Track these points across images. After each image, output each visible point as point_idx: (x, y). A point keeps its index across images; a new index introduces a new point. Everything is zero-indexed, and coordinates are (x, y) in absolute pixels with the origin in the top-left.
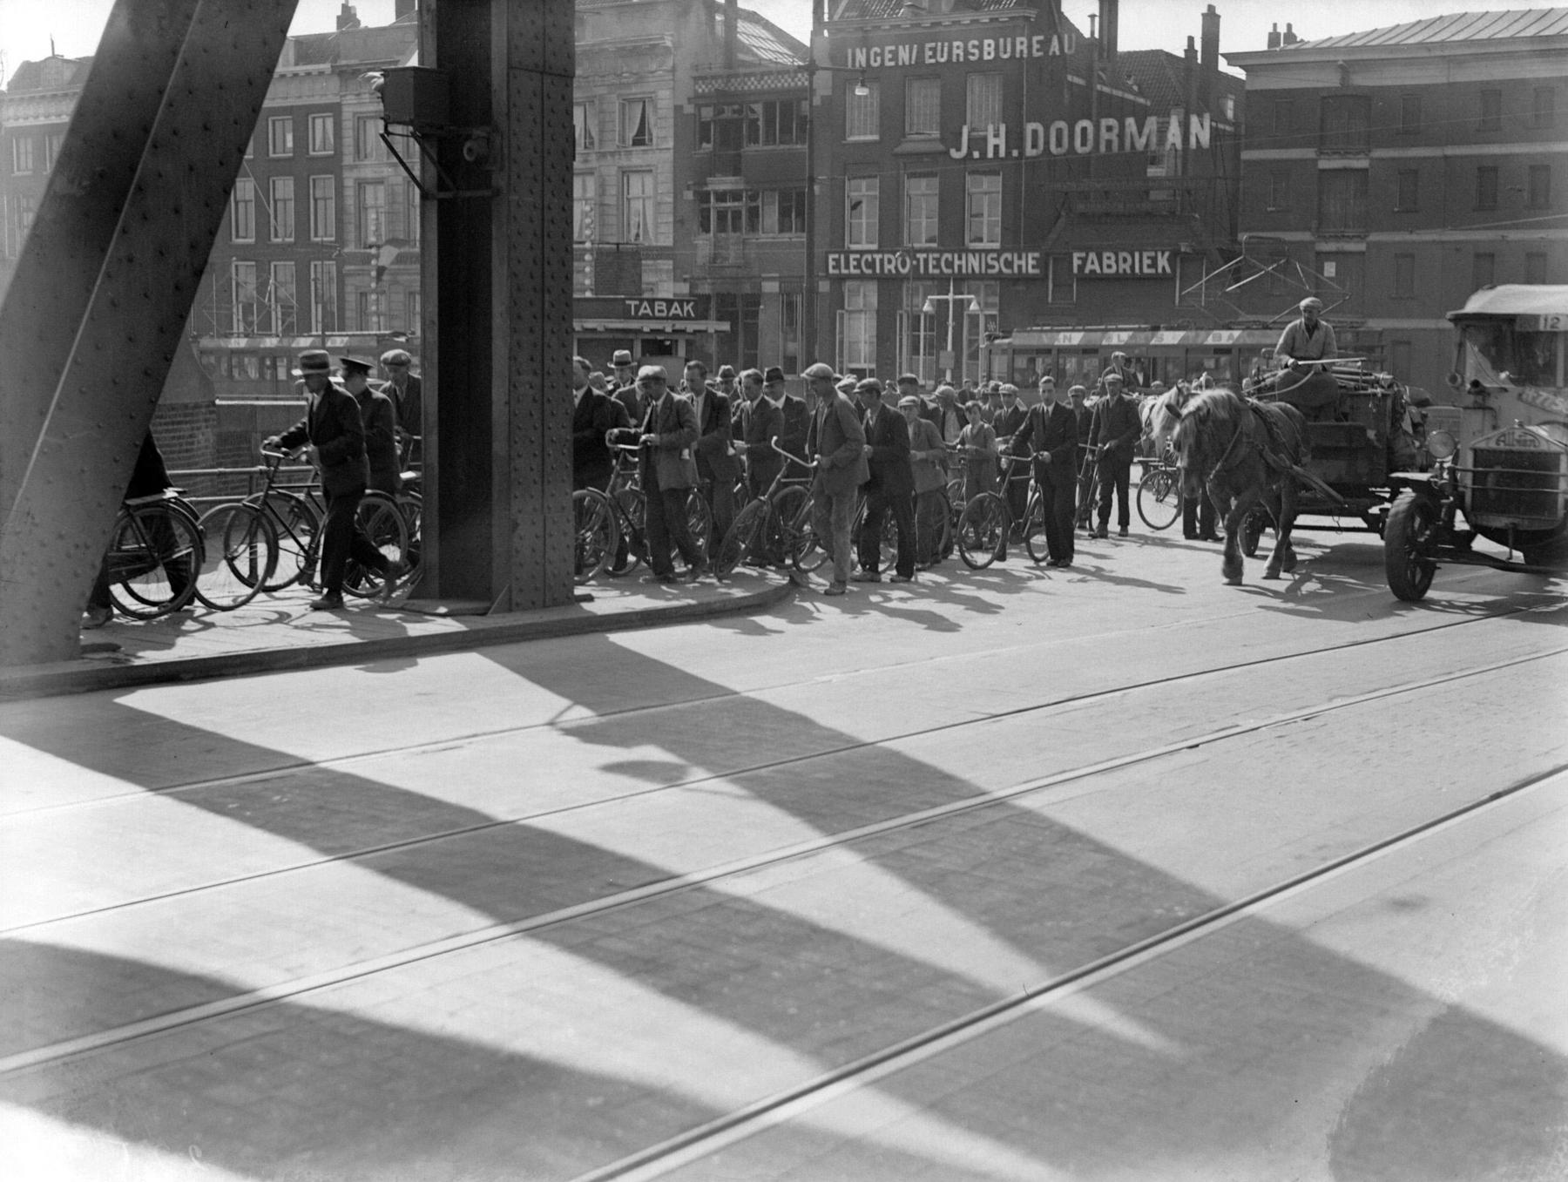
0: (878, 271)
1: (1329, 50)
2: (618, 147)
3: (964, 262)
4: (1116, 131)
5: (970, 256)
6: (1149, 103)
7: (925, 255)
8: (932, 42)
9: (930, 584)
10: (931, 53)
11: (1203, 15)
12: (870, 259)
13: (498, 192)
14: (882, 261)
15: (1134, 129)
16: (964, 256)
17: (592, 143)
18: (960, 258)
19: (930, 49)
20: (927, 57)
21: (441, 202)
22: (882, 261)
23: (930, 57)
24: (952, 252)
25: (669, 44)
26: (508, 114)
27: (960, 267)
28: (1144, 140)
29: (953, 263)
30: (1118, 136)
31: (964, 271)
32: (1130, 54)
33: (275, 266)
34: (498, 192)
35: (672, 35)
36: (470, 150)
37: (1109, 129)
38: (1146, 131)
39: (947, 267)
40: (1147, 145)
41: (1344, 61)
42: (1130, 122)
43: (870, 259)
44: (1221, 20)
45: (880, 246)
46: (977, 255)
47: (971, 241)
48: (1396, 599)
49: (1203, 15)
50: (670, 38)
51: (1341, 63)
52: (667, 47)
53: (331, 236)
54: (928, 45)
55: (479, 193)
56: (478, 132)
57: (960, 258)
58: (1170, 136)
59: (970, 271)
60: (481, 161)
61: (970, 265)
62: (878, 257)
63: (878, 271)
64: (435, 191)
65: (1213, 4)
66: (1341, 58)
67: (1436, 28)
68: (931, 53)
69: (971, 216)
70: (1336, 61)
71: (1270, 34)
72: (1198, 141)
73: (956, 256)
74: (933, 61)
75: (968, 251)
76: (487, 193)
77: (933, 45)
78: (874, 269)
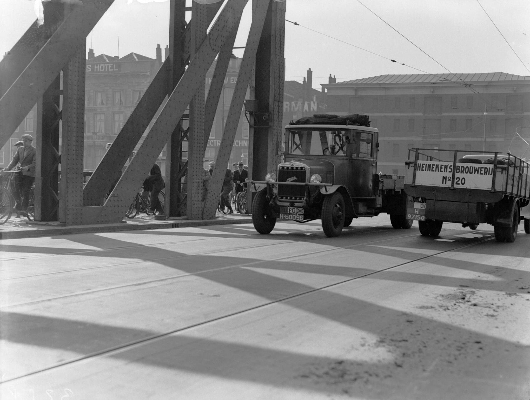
0: (215, 145)
1: (351, 84)
2: (131, 105)
3: (242, 143)
4: (289, 105)
5: (244, 141)
6: (294, 97)
7: (216, 141)
8: (233, 77)
9: (289, 234)
10: (232, 80)
11: (307, 71)
12: (213, 142)
13: (270, 127)
14: (216, 142)
15: (294, 105)
16: (242, 141)
17: (123, 104)
18: (241, 142)
19: (232, 79)
20: (231, 81)
21: (255, 128)
22: (216, 142)
23: (232, 82)
24: (239, 140)
25: (148, 74)
26: (274, 110)
27: (241, 144)
28: (297, 108)
29: (238, 143)
30: (289, 107)
31: (242, 146)
32: (287, 81)
33: (11, 140)
34: (270, 127)
35: (149, 72)
36: (265, 117)
37: (287, 105)
38: (298, 106)
39: (212, 144)
40: (298, 110)
41: (356, 88)
42: (293, 103)
43: (213, 142)
44: (313, 73)
45: (216, 138)
46: (246, 141)
47: (244, 137)
48: (421, 234)
49: (307, 71)
50: (149, 72)
51: (355, 88)
52: (148, 75)
53: (32, 130)
54: (232, 78)
55: (265, 126)
56: (267, 114)
57: (241, 142)
58: (305, 107)
59: (244, 146)
60: (267, 120)
61: (244, 144)
62: (215, 141)
63: (215, 145)
64: (253, 126)
65: (310, 68)
66: (355, 87)
67: (380, 79)
68: (232, 80)
69: (244, 129)
70: (354, 87)
71: (329, 77)
72: (313, 110)
73: (240, 141)
74: (233, 83)
75: (243, 140)
76: (267, 127)
77: (233, 78)
78: (214, 145)
